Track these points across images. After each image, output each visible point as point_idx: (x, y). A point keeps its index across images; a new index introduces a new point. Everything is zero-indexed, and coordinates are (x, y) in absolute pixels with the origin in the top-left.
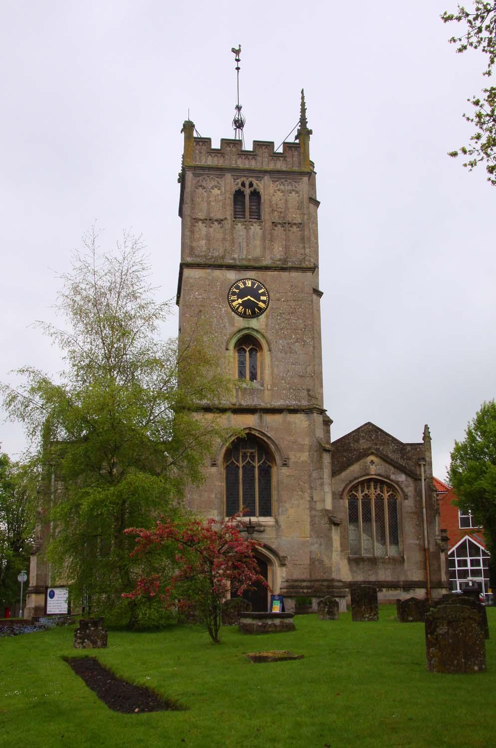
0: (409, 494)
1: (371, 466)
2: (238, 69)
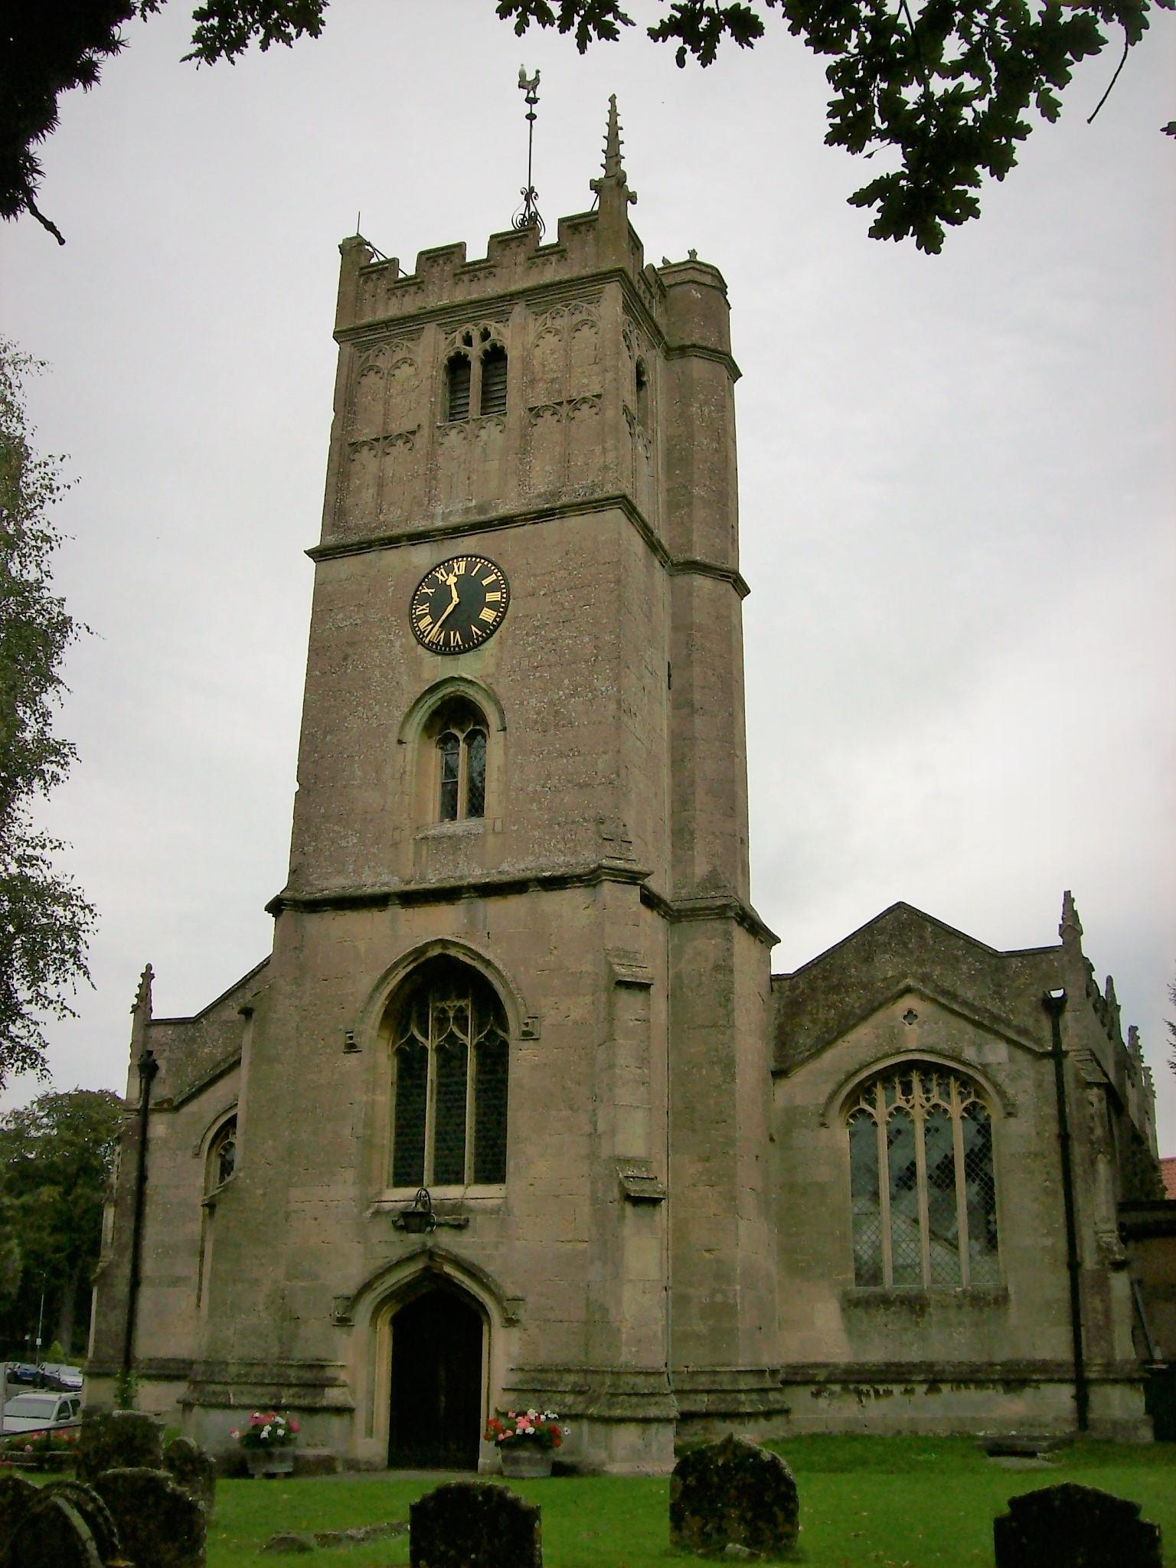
0: (1022, 1099)
1: (908, 1027)
2: (531, 117)
